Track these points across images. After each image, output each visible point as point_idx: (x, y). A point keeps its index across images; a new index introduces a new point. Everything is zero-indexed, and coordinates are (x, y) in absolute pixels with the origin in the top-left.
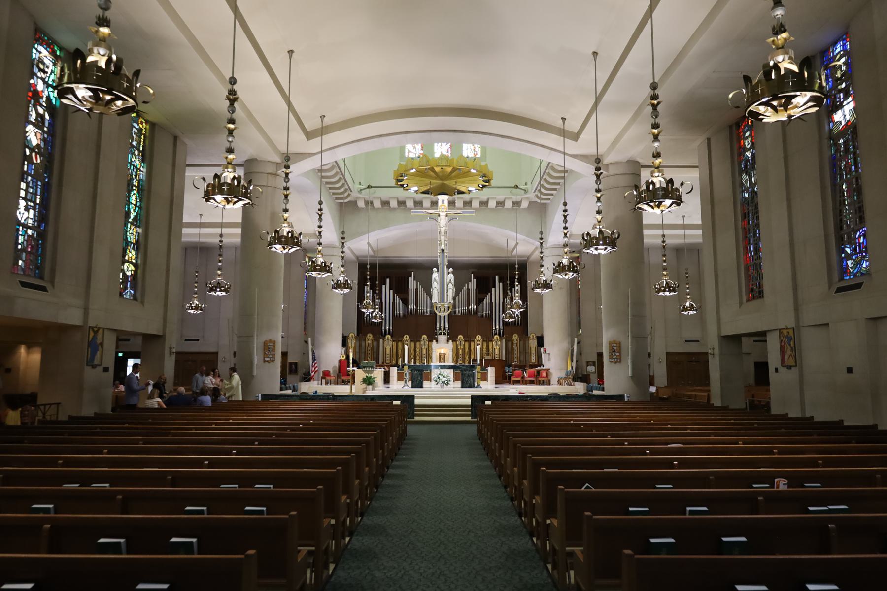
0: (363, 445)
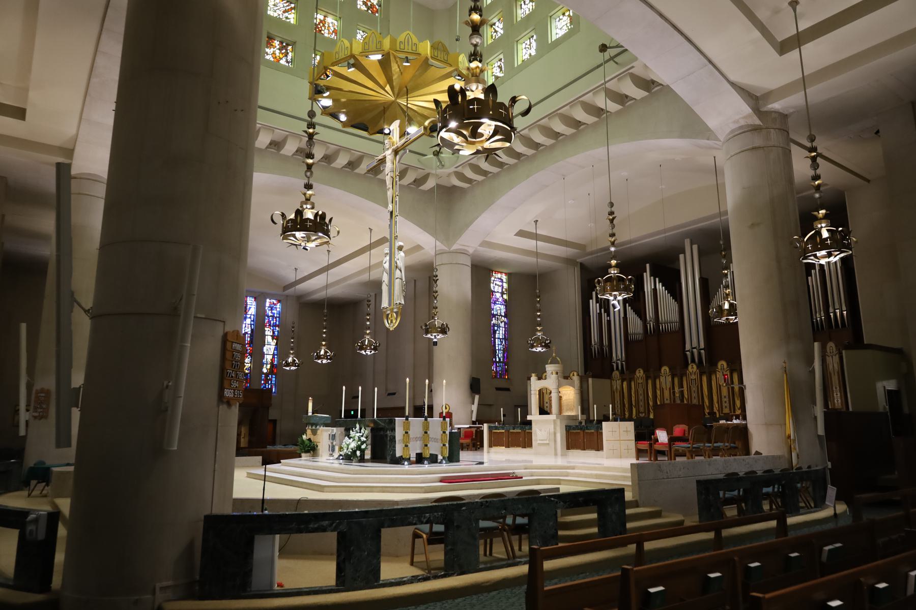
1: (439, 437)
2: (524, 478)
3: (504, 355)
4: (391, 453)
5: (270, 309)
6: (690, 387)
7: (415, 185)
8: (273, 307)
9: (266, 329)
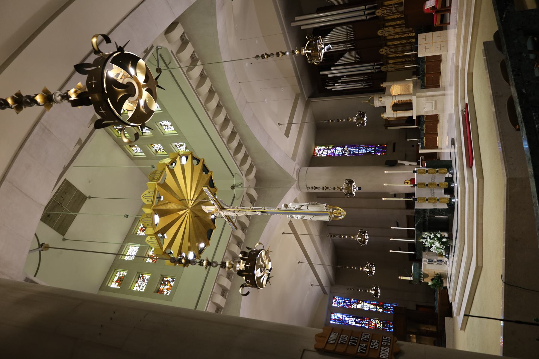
1: (431, 175)
2: (467, 102)
3: (370, 148)
4: (445, 213)
5: (339, 304)
6: (395, 52)
7: (254, 203)
8: (338, 302)
9: (352, 307)
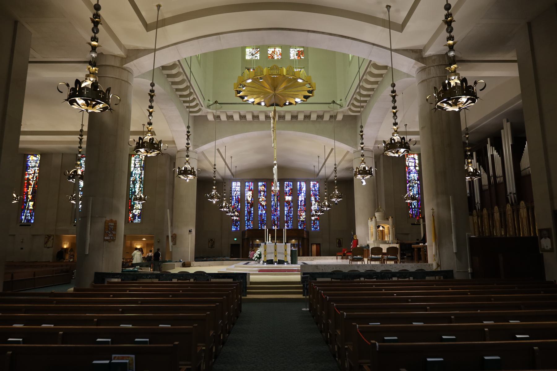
0: (234, 287)
3: (418, 204)
